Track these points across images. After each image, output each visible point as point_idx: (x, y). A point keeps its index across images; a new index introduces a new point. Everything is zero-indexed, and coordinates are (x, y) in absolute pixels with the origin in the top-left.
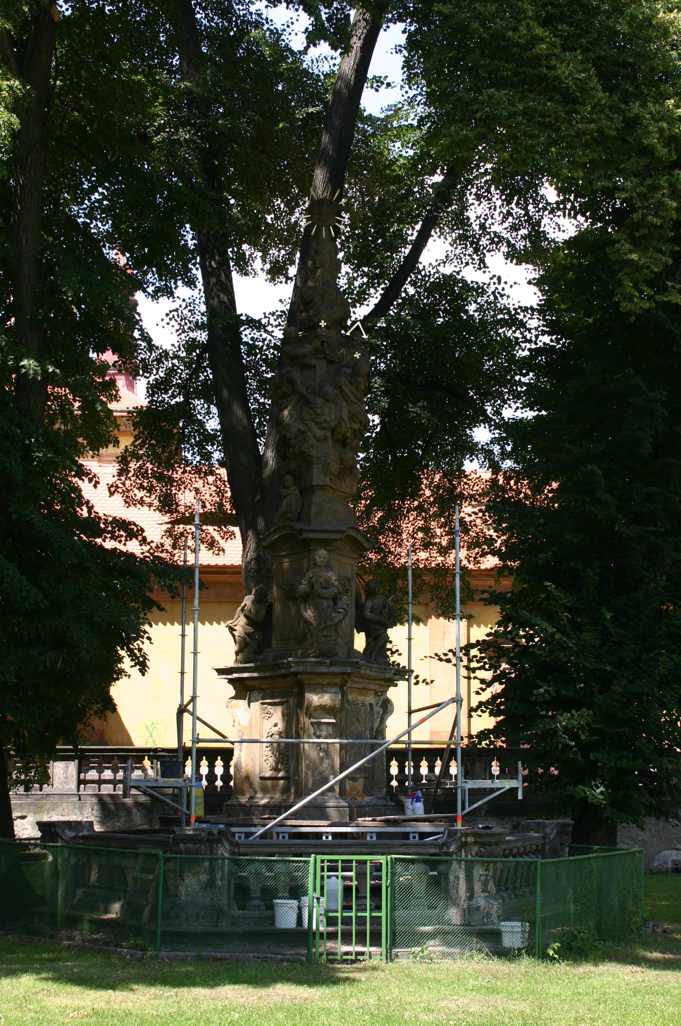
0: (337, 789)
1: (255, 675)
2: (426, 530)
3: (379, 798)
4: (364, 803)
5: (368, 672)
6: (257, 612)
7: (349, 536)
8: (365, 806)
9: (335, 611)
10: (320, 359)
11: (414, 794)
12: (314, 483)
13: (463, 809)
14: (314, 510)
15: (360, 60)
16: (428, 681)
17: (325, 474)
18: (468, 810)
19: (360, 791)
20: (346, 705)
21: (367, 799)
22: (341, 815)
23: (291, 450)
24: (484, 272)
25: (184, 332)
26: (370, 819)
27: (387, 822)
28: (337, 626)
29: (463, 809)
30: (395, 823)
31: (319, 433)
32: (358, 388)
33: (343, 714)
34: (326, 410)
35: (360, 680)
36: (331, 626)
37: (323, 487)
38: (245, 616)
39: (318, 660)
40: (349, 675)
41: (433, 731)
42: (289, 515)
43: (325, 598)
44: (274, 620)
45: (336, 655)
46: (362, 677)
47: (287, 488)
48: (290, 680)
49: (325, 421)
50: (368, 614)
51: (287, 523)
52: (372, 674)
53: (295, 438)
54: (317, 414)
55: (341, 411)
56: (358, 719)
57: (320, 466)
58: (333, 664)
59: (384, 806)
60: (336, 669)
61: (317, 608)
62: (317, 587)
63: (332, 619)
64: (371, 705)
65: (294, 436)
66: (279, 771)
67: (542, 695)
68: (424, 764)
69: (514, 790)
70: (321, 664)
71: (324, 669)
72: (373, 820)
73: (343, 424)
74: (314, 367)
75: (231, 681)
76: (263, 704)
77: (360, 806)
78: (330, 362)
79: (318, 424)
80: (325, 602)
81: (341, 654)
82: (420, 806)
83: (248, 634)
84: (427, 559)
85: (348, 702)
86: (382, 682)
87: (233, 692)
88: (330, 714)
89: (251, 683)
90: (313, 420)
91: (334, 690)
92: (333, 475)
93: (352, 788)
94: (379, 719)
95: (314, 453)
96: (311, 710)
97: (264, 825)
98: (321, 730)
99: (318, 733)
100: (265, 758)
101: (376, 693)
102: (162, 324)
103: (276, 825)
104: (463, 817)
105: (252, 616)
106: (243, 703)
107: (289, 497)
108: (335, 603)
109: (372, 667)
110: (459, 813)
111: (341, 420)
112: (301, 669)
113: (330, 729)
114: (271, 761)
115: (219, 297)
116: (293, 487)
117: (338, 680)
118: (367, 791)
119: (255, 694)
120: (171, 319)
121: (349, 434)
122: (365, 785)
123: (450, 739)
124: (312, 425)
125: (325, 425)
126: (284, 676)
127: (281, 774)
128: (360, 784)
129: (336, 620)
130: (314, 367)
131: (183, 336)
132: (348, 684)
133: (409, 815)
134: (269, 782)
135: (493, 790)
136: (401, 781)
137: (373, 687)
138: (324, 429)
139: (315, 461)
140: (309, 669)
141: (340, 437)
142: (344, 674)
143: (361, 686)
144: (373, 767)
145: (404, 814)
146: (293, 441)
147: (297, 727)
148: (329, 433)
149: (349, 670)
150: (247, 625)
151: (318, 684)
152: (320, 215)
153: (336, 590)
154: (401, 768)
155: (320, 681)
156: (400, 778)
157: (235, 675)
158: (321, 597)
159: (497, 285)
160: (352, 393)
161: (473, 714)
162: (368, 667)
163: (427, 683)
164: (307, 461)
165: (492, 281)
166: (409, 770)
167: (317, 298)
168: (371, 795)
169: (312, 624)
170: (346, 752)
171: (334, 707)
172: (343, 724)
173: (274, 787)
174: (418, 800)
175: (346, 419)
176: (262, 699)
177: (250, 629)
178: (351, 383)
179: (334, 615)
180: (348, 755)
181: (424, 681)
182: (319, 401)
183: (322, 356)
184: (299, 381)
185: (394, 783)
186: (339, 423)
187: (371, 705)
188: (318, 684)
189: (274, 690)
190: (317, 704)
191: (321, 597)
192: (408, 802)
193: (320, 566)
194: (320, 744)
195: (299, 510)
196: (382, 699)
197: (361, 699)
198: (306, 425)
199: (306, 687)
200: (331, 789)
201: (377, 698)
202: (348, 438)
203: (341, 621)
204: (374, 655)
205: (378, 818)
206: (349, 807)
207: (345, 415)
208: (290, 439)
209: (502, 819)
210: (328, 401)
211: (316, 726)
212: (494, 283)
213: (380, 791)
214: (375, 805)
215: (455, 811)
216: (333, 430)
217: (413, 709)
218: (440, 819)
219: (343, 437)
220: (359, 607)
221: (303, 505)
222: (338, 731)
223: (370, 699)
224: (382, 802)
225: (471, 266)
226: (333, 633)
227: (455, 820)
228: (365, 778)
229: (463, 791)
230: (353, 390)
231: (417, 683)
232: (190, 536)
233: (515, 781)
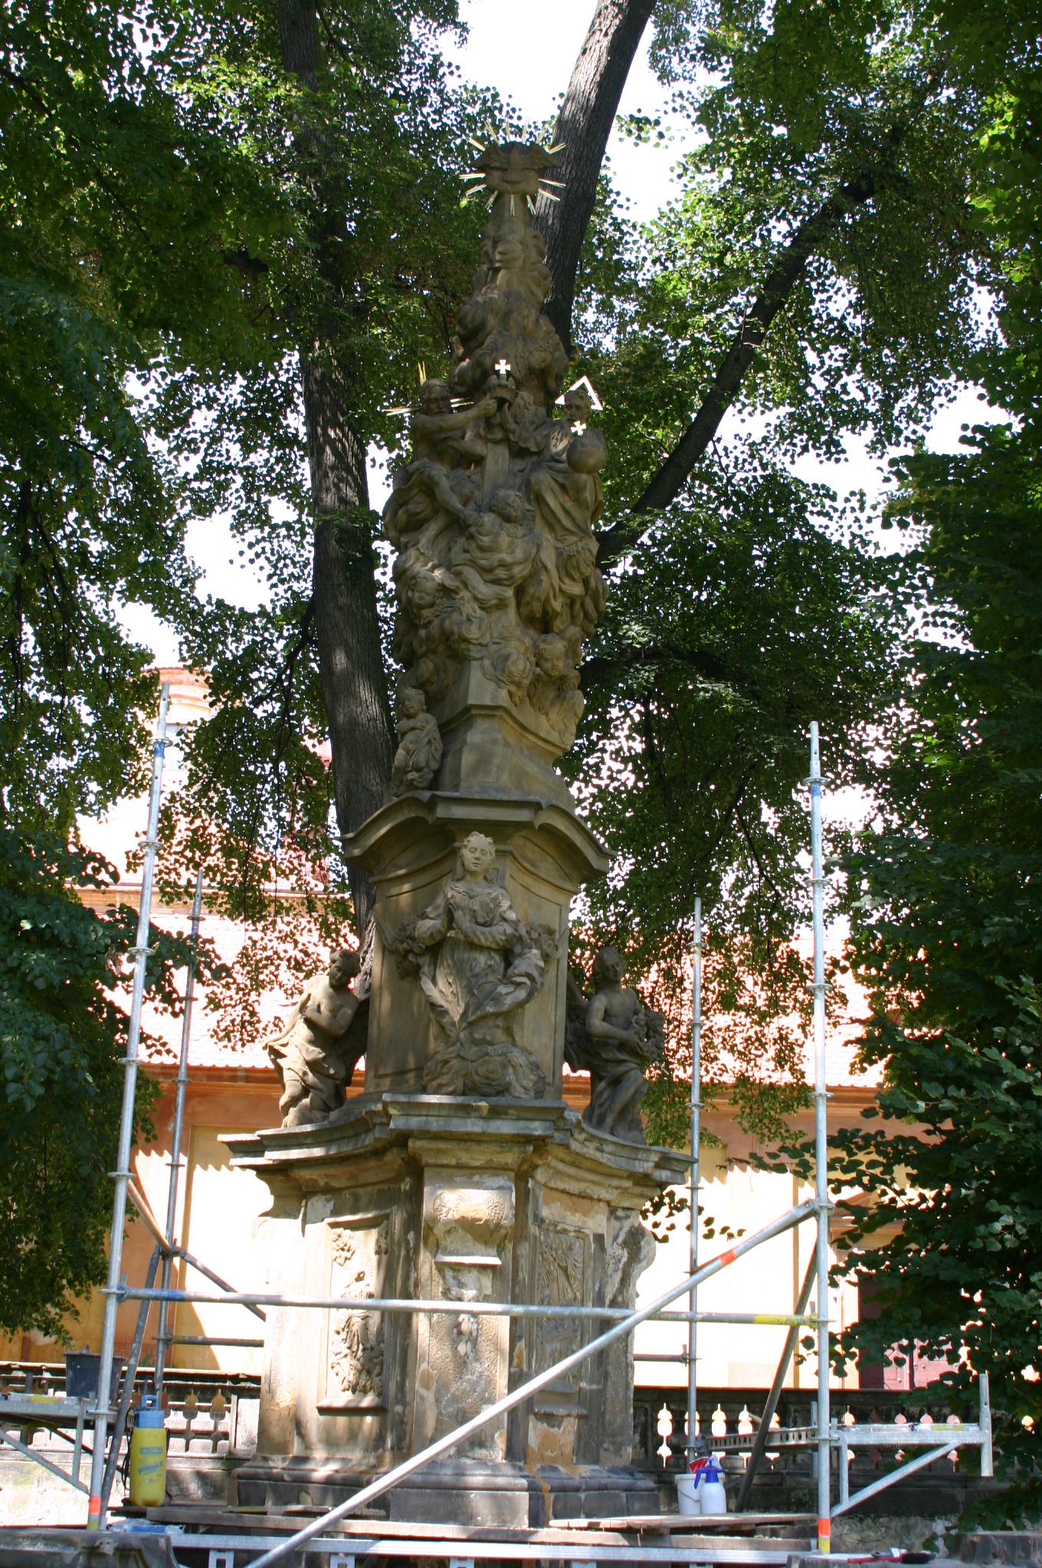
0: (500, 1442)
1: (318, 1152)
2: (727, 974)
3: (614, 1470)
4: (577, 1481)
5: (590, 1150)
6: (334, 1011)
7: (548, 831)
8: (577, 1489)
9: (506, 979)
10: (496, 442)
11: (701, 1463)
12: (471, 701)
13: (835, 1500)
14: (467, 759)
15: (607, 68)
16: (734, 1230)
17: (498, 682)
18: (847, 1503)
19: (568, 1450)
20: (534, 1229)
21: (585, 1470)
22: (503, 1509)
23: (422, 633)
24: (837, 461)
25: (282, 581)
26: (584, 1522)
27: (628, 1532)
28: (509, 1017)
29: (835, 1500)
30: (652, 1536)
31: (485, 590)
32: (579, 502)
33: (524, 1249)
34: (504, 540)
35: (572, 1171)
36: (496, 1015)
37: (491, 711)
38: (309, 1022)
39: (460, 1099)
40: (540, 1144)
41: (741, 1359)
42: (411, 776)
43: (481, 948)
44: (373, 1030)
45: (504, 1090)
46: (577, 1161)
47: (409, 717)
48: (393, 1157)
49: (502, 564)
50: (597, 1024)
51: (410, 794)
52: (604, 1158)
53: (432, 605)
54: (482, 549)
55: (539, 547)
56: (565, 1270)
57: (487, 663)
58: (495, 1113)
59: (628, 1489)
60: (505, 1127)
61: (460, 971)
62: (463, 919)
63: (497, 999)
64: (599, 1238)
65: (428, 599)
66: (365, 1391)
67: (999, 1237)
68: (719, 1417)
69: (970, 1453)
70: (465, 1110)
71: (473, 1125)
72: (592, 1527)
73: (544, 577)
74: (479, 461)
75: (262, 1171)
76: (333, 1225)
77: (563, 1489)
78: (519, 452)
79: (484, 571)
80: (482, 959)
81: (518, 1091)
82: (715, 1493)
83: (312, 1065)
84: (728, 1029)
85: (539, 1221)
86: (627, 1184)
87: (268, 1201)
88: (486, 1243)
89: (306, 1174)
90: (472, 563)
91: (501, 1181)
92: (519, 685)
93: (546, 1441)
94: (619, 1275)
95: (473, 633)
96: (439, 1231)
97: (290, 1533)
98: (461, 1285)
99: (454, 1291)
100: (333, 1359)
101: (613, 1211)
102: (239, 561)
103: (322, 1533)
104: (833, 1520)
105: (324, 1018)
106: (290, 1226)
107: (410, 737)
108: (508, 964)
109: (602, 1141)
110: (825, 1511)
111: (538, 568)
112: (414, 1122)
113: (487, 1282)
114: (347, 1369)
115: (339, 489)
116: (422, 716)
117: (510, 1158)
118: (587, 1449)
119: (318, 1203)
120: (258, 555)
121: (557, 605)
122: (579, 1436)
123: (799, 1309)
124: (470, 574)
125: (501, 573)
126: (378, 1153)
127: (367, 1401)
128: (567, 1432)
129: (509, 1001)
130: (479, 461)
131: (281, 589)
132: (540, 1175)
133: (690, 1515)
134: (342, 1420)
135: (915, 1451)
136: (677, 1449)
137: (604, 1194)
138: (497, 582)
139: (474, 652)
140: (435, 1124)
141: (537, 607)
142: (527, 1139)
143: (574, 1187)
144: (602, 1392)
145: (677, 1512)
146: (426, 613)
147: (406, 1277)
148: (509, 593)
149: (537, 1128)
150: (311, 1042)
151: (460, 1166)
152: (504, 170)
153: (509, 930)
154: (678, 1423)
155: (465, 1158)
156: (674, 1441)
157: (271, 1157)
158: (472, 946)
159: (858, 514)
160: (567, 512)
161: (838, 1278)
162: (592, 1138)
163: (731, 1236)
164: (455, 652)
165: (848, 505)
166: (693, 1427)
167: (492, 321)
168: (596, 1462)
169: (446, 1012)
170: (530, 1347)
171: (498, 1226)
172: (524, 1275)
173: (353, 1435)
174: (711, 1477)
175: (551, 566)
176: (335, 1213)
177: (316, 1053)
178: (563, 487)
179: (503, 989)
180: (529, 1343)
181: (724, 1230)
182: (488, 519)
183: (499, 435)
184: (445, 483)
185: (665, 1451)
186: (534, 576)
187: (599, 1238)
188: (460, 1166)
189: (361, 1191)
190: (455, 1215)
191: (472, 946)
192: (686, 1482)
193: (473, 873)
194: (467, 1322)
195: (434, 766)
196: (627, 1225)
197: (573, 1220)
198: (458, 574)
199: (427, 1174)
200: (477, 1441)
201: (616, 1224)
202: (557, 614)
203: (521, 1005)
204: (609, 1121)
205: (606, 1522)
206: (532, 1489)
207: (548, 557)
208: (420, 607)
209: (861, 1520)
210: (507, 519)
211: (449, 1274)
212: (853, 510)
213: (618, 1451)
214: (605, 1487)
215: (809, 1503)
216: (520, 592)
217: (700, 1327)
218: (773, 1529)
219: (545, 613)
220: (576, 1013)
221: (444, 755)
222: (509, 1284)
223: (597, 1222)
224: (624, 1480)
225: (812, 452)
226: (500, 1035)
227: (809, 1532)
228: (580, 1417)
229: (836, 1451)
230: (569, 504)
231: (710, 1235)
232: (284, 964)
233: (972, 1428)
